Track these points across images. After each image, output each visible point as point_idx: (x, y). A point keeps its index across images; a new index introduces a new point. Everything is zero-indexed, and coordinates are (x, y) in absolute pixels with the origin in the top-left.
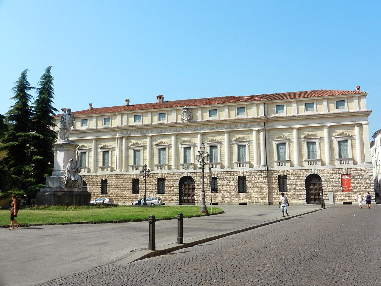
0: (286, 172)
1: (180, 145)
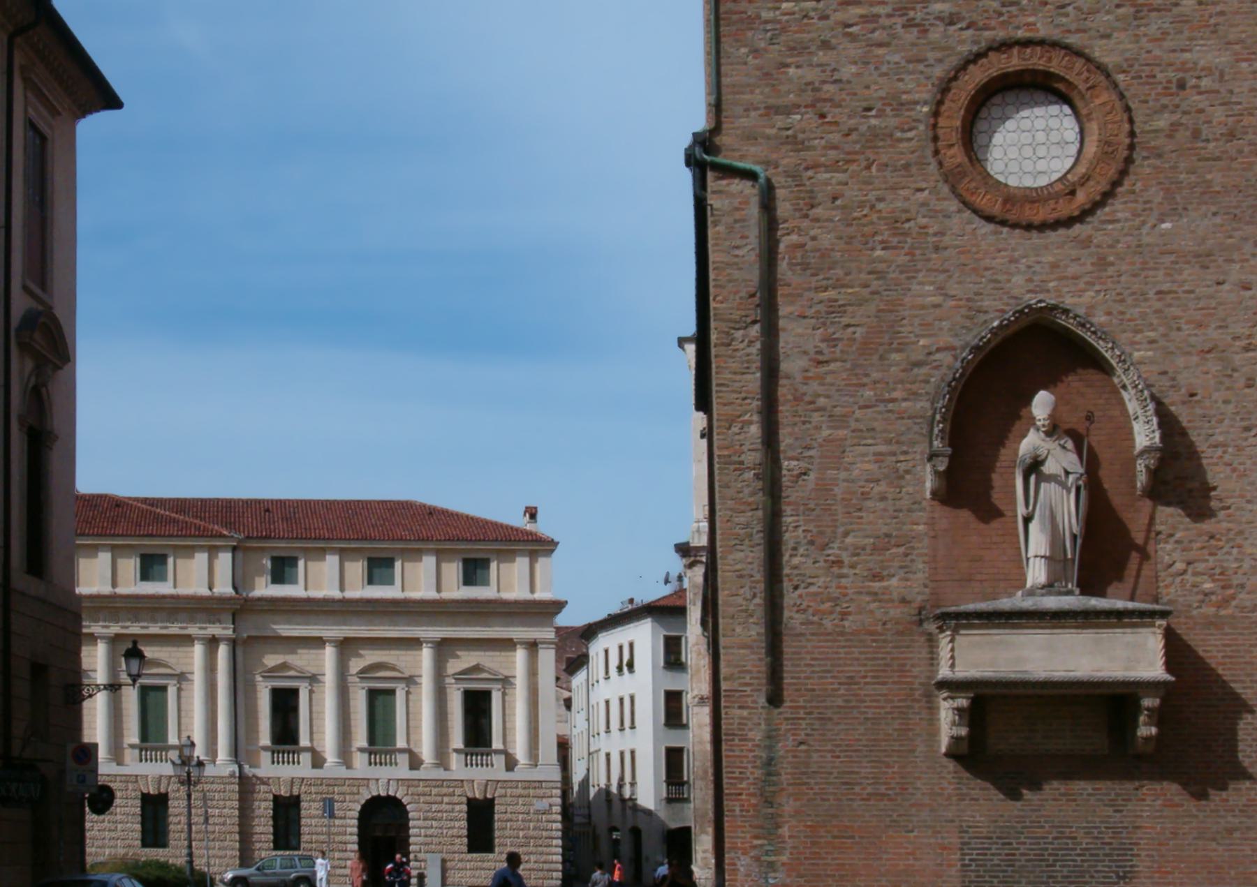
0: (164, 782)
1: (259, 678)
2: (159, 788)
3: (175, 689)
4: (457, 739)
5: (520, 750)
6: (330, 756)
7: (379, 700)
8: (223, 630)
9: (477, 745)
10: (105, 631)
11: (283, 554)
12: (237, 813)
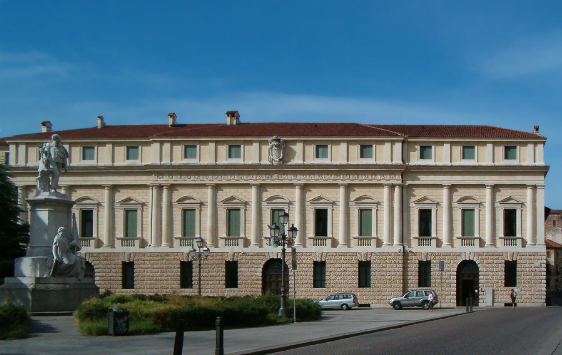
0: (369, 255)
2: (233, 259)
3: (331, 210)
4: (501, 232)
5: (528, 238)
6: (445, 242)
7: (467, 214)
8: (397, 180)
9: (85, 236)
10: (254, 182)
11: (424, 145)
12: (402, 269)
